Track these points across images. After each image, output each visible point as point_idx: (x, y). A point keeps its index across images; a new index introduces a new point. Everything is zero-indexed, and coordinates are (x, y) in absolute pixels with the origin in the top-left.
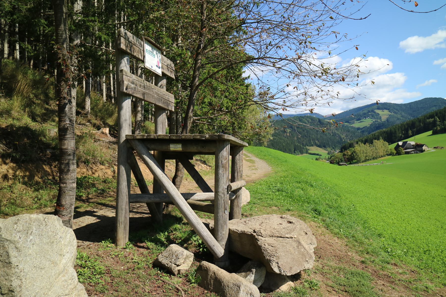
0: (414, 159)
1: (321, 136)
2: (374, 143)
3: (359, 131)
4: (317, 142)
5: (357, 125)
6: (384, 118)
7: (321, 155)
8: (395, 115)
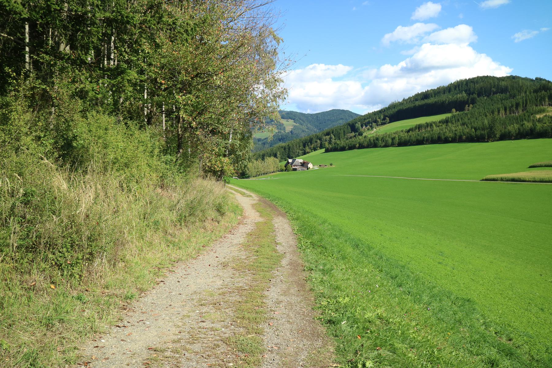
0: (301, 173)
2: (265, 160)
3: (260, 143)
8: (301, 127)
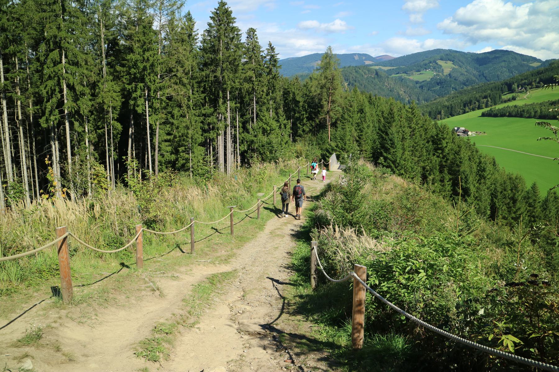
3: (418, 85)
5: (416, 77)
6: (447, 71)
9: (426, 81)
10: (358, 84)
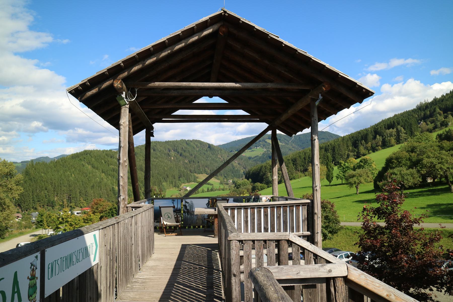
1: (211, 163)
4: (207, 169)
7: (212, 185)
9: (258, 156)
10: (188, 155)
